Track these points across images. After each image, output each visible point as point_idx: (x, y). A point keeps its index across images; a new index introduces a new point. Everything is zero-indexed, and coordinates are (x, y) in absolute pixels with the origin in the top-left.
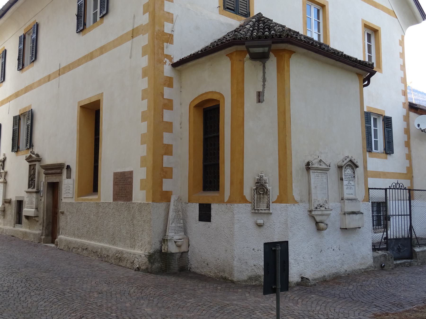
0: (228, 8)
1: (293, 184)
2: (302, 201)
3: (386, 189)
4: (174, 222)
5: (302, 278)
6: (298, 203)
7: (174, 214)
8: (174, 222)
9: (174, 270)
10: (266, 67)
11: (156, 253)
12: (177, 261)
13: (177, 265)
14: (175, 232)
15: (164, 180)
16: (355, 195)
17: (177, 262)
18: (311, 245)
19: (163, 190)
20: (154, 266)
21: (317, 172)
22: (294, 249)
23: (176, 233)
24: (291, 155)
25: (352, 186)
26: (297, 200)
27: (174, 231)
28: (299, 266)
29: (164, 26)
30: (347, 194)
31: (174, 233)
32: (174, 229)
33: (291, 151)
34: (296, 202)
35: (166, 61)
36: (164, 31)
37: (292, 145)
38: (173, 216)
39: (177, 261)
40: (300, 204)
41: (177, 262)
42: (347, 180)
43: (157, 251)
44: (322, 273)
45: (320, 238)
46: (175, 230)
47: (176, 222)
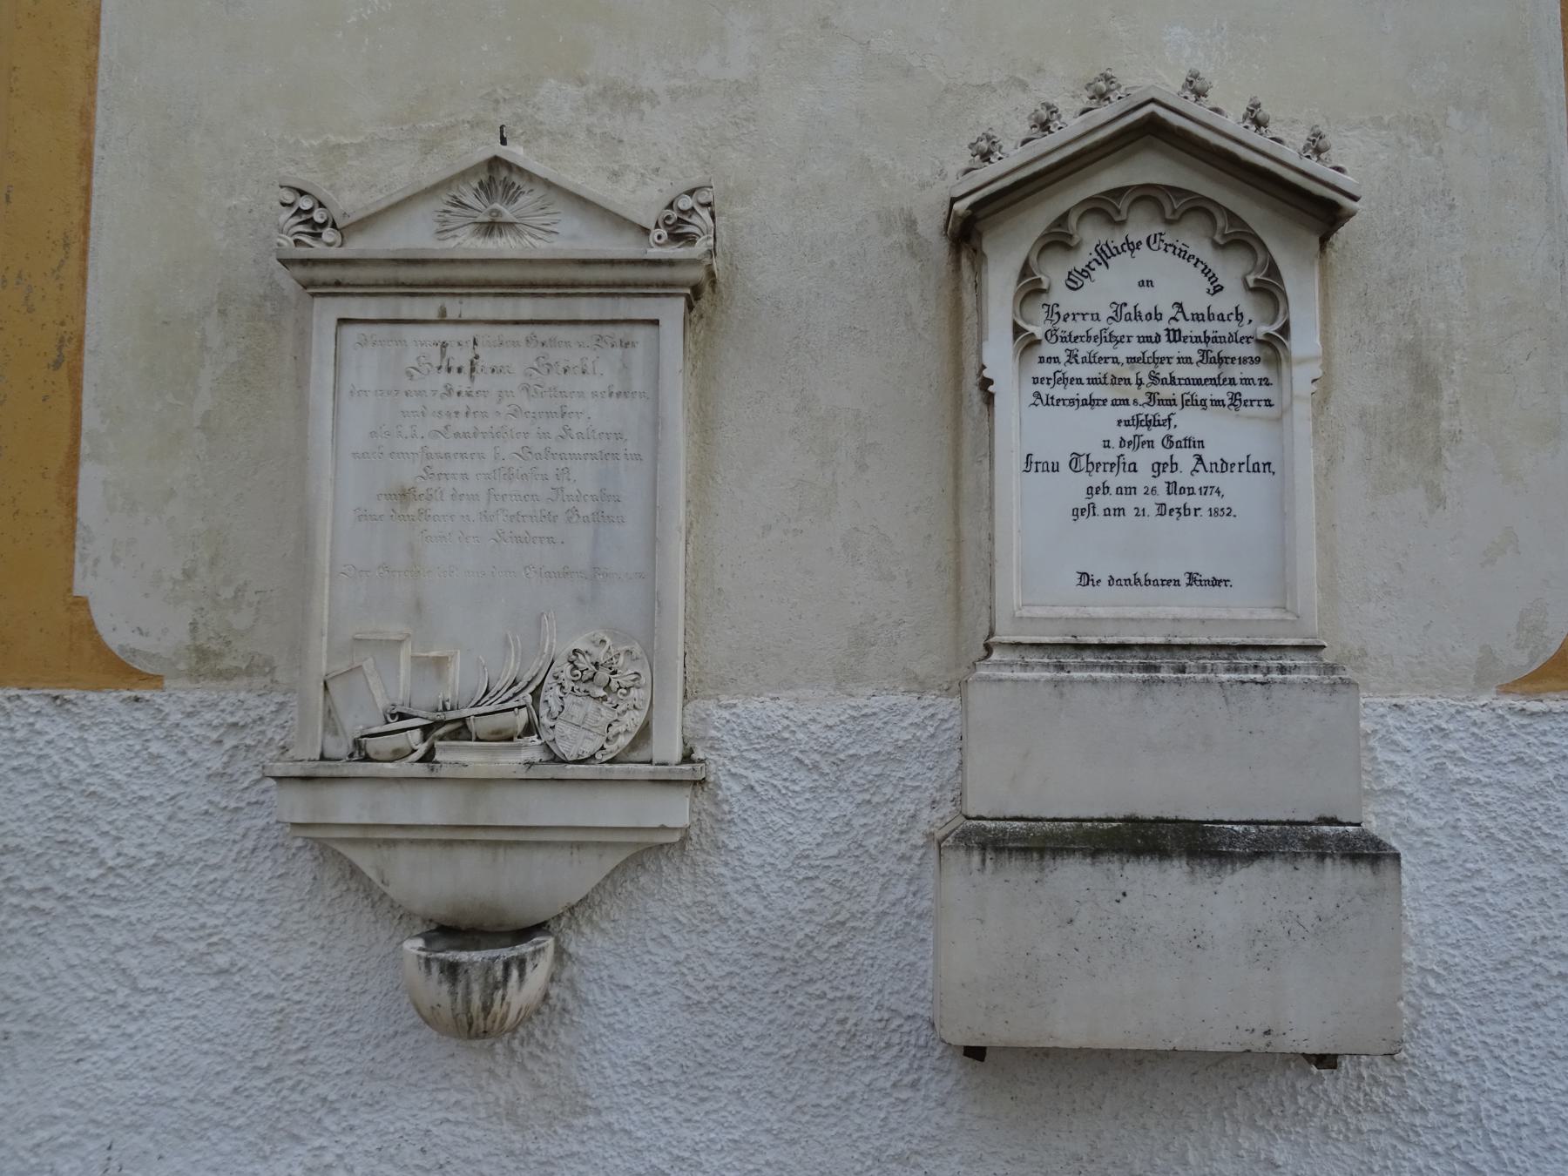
1: (88, 472)
2: (227, 663)
6: (155, 681)
16: (1282, 586)
21: (443, 320)
24: (86, 157)
25: (1225, 466)
26: (136, 642)
30: (1086, 579)
33: (86, 120)
37: (108, 49)
42: (1091, 402)
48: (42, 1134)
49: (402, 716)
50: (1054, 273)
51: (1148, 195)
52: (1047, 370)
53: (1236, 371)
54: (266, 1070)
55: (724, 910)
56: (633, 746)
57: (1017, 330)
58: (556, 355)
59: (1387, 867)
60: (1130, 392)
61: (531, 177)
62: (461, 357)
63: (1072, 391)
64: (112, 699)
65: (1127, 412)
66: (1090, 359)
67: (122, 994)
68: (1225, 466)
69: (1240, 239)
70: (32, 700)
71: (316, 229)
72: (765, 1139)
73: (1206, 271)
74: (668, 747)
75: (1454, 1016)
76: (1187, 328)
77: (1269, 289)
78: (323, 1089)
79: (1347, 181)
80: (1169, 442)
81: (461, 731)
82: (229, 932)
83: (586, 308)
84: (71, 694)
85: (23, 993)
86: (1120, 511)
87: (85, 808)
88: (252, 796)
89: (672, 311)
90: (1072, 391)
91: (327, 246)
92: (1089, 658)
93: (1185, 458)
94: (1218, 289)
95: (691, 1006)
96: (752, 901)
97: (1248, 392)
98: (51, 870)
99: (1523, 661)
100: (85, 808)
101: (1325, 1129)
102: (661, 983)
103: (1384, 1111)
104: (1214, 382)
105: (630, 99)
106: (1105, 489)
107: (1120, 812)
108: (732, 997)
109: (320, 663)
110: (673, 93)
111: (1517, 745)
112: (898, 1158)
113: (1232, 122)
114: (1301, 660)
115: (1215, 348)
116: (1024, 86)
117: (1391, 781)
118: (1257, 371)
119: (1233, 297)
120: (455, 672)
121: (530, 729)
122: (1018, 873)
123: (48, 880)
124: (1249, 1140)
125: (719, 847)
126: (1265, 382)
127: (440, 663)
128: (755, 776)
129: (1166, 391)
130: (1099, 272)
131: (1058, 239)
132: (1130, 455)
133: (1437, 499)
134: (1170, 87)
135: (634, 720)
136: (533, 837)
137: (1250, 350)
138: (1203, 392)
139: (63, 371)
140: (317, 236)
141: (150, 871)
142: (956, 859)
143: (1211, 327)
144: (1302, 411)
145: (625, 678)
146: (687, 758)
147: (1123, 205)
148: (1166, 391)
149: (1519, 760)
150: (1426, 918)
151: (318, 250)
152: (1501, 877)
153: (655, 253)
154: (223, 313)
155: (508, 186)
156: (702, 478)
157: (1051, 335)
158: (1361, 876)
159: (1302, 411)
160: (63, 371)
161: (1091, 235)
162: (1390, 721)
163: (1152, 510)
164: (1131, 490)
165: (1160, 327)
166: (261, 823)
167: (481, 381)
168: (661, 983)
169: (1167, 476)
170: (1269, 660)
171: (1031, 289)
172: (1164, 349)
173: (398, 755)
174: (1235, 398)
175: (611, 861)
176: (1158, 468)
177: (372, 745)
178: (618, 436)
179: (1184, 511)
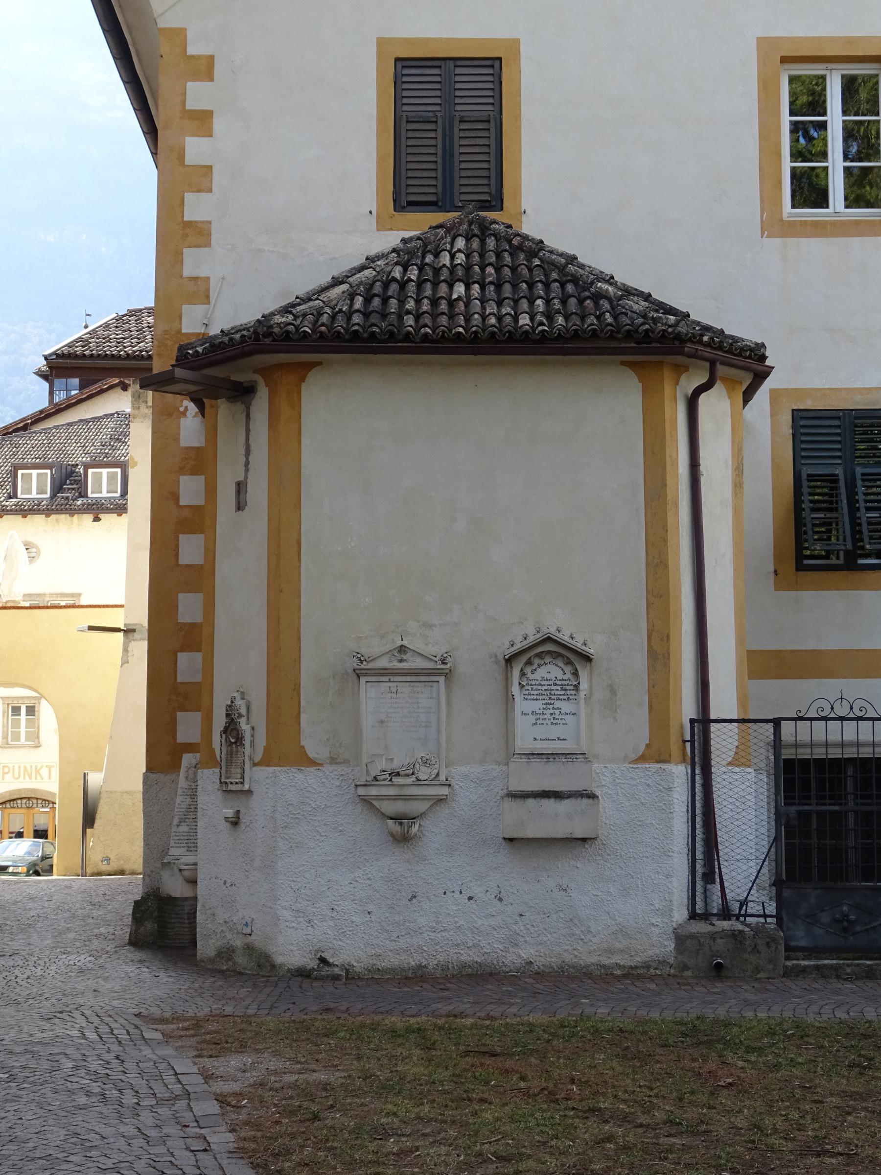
0: (411, 203)
1: (304, 717)
2: (338, 760)
3: (777, 723)
4: (187, 820)
5: (323, 961)
6: (322, 765)
7: (188, 800)
8: (185, 822)
9: (178, 941)
10: (251, 416)
11: (152, 898)
12: (188, 919)
13: (187, 930)
14: (188, 847)
15: (179, 714)
17: (187, 921)
18: (368, 879)
19: (178, 741)
20: (142, 929)
21: (390, 681)
22: (293, 884)
23: (192, 849)
24: (299, 639)
25: (566, 714)
26: (316, 756)
27: (184, 845)
28: (310, 929)
29: (180, 317)
30: (535, 739)
31: (186, 848)
32: (186, 838)
34: (313, 763)
35: (186, 408)
36: (181, 330)
38: (185, 807)
39: (188, 919)
40: (328, 768)
41: (187, 921)
42: (537, 699)
43: (154, 892)
44: (412, 957)
45: (408, 861)
46: (189, 841)
47: (191, 820)
48: (301, 869)
49: (384, 771)
50: (528, 670)
51: (549, 653)
52: (527, 692)
53: (569, 692)
54: (351, 853)
55: (456, 814)
56: (435, 777)
57: (520, 684)
58: (416, 689)
59: (596, 799)
60: (545, 697)
61: (410, 649)
62: (394, 690)
63: (532, 697)
64: (312, 769)
65: (544, 702)
66: (536, 690)
67: (318, 837)
68: (566, 714)
69: (569, 662)
70: (293, 770)
71: (362, 662)
72: (466, 865)
73: (562, 669)
74: (442, 778)
75: (616, 835)
76: (558, 682)
77: (576, 674)
78: (365, 857)
79: (592, 651)
80: (554, 708)
81: (398, 774)
82: (342, 822)
83: (422, 678)
84: (303, 768)
85: (295, 837)
86: (543, 724)
87: (307, 795)
88: (346, 791)
89: (442, 679)
90: (532, 697)
91: (364, 666)
92: (535, 756)
93: (557, 712)
94: (565, 674)
95: (448, 836)
96: (462, 812)
97: (571, 697)
98: (300, 809)
99: (634, 756)
100: (307, 795)
101: (589, 860)
102: (441, 831)
103: (601, 855)
104: (564, 695)
105: (429, 626)
106: (539, 719)
107: (541, 789)
108: (457, 834)
109: (365, 759)
110: (440, 624)
111: (631, 775)
112: (495, 868)
113: (566, 638)
114: (581, 756)
115: (564, 687)
116: (522, 623)
117: (604, 783)
118: (573, 692)
119: (569, 675)
120: (395, 761)
121: (413, 774)
122: (519, 802)
123: (299, 811)
124: (572, 862)
125: (454, 800)
126: (575, 695)
127: (392, 760)
128: (462, 784)
129: (553, 697)
130: (538, 670)
131: (529, 663)
132: (545, 711)
133: (615, 720)
134: (553, 630)
135: (436, 771)
136: (413, 797)
137: (572, 688)
138: (561, 697)
139: (296, 692)
140: (362, 663)
141: (323, 808)
142: (506, 799)
143: (563, 682)
144: (582, 702)
145: (433, 762)
146: (447, 780)
147: (543, 655)
148: (553, 697)
149: (632, 778)
150: (611, 813)
151: (362, 666)
152: (627, 804)
153: (438, 667)
154: (334, 677)
155: (405, 651)
156: (449, 716)
157: (528, 684)
158: (590, 801)
159: (582, 702)
160: (296, 692)
161: (537, 661)
162: (604, 770)
163: (550, 724)
164: (545, 719)
165: (552, 682)
166: (348, 797)
167: (399, 695)
168: (441, 831)
169: (553, 716)
170: (574, 757)
171: (523, 674)
172: (553, 687)
173: (384, 780)
174: (568, 698)
175: (431, 803)
176: (551, 714)
177: (378, 778)
178: (430, 708)
179: (557, 724)
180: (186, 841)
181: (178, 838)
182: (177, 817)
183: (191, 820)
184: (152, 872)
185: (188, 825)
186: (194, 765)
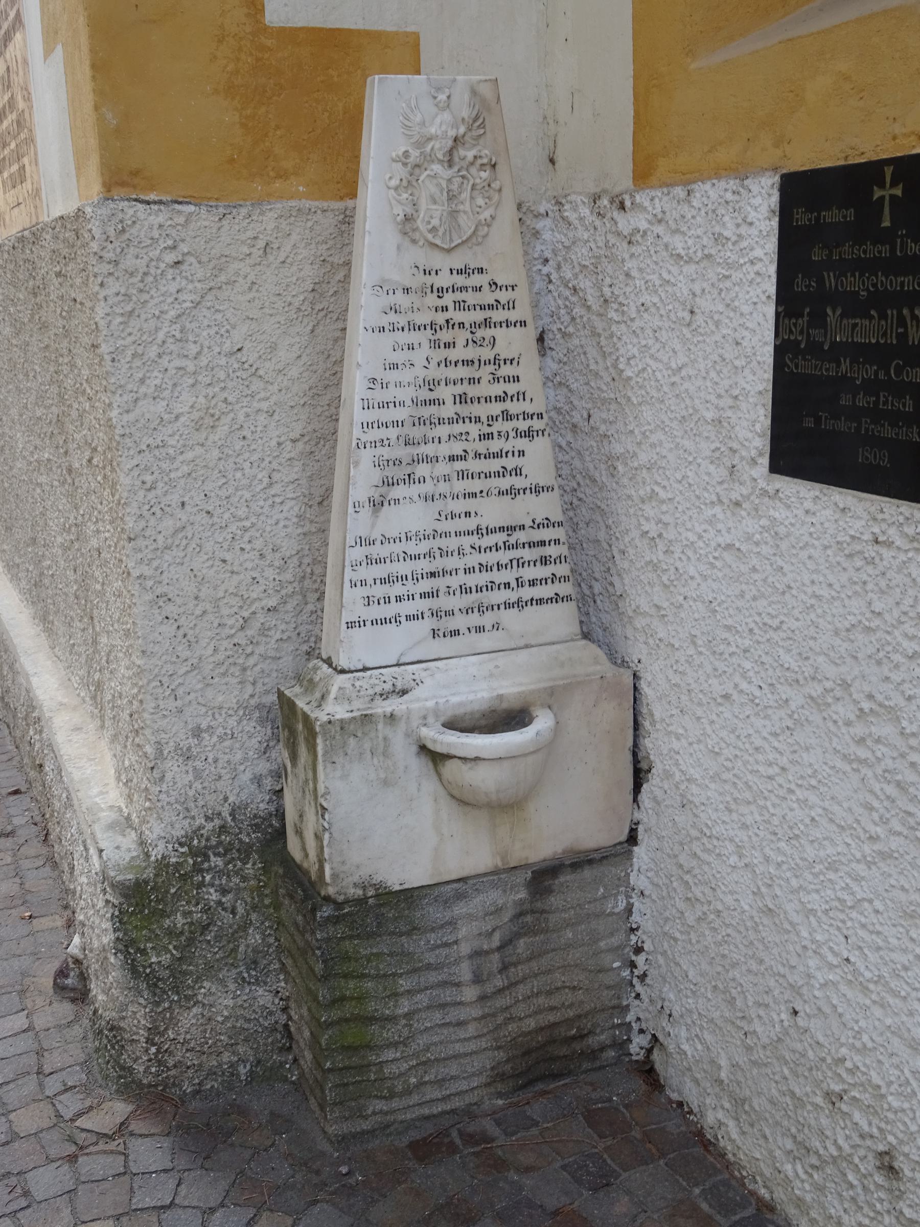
4: (422, 470)
7: (419, 357)
11: (217, 861)
12: (478, 979)
14: (435, 614)
27: (423, 605)
31: (428, 624)
32: (424, 566)
38: (406, 394)
46: (440, 583)
47: (443, 468)
180: (426, 585)
181: (379, 571)
182: (367, 456)
183: (443, 468)
184: (197, 732)
185: (429, 498)
186: (440, 147)
